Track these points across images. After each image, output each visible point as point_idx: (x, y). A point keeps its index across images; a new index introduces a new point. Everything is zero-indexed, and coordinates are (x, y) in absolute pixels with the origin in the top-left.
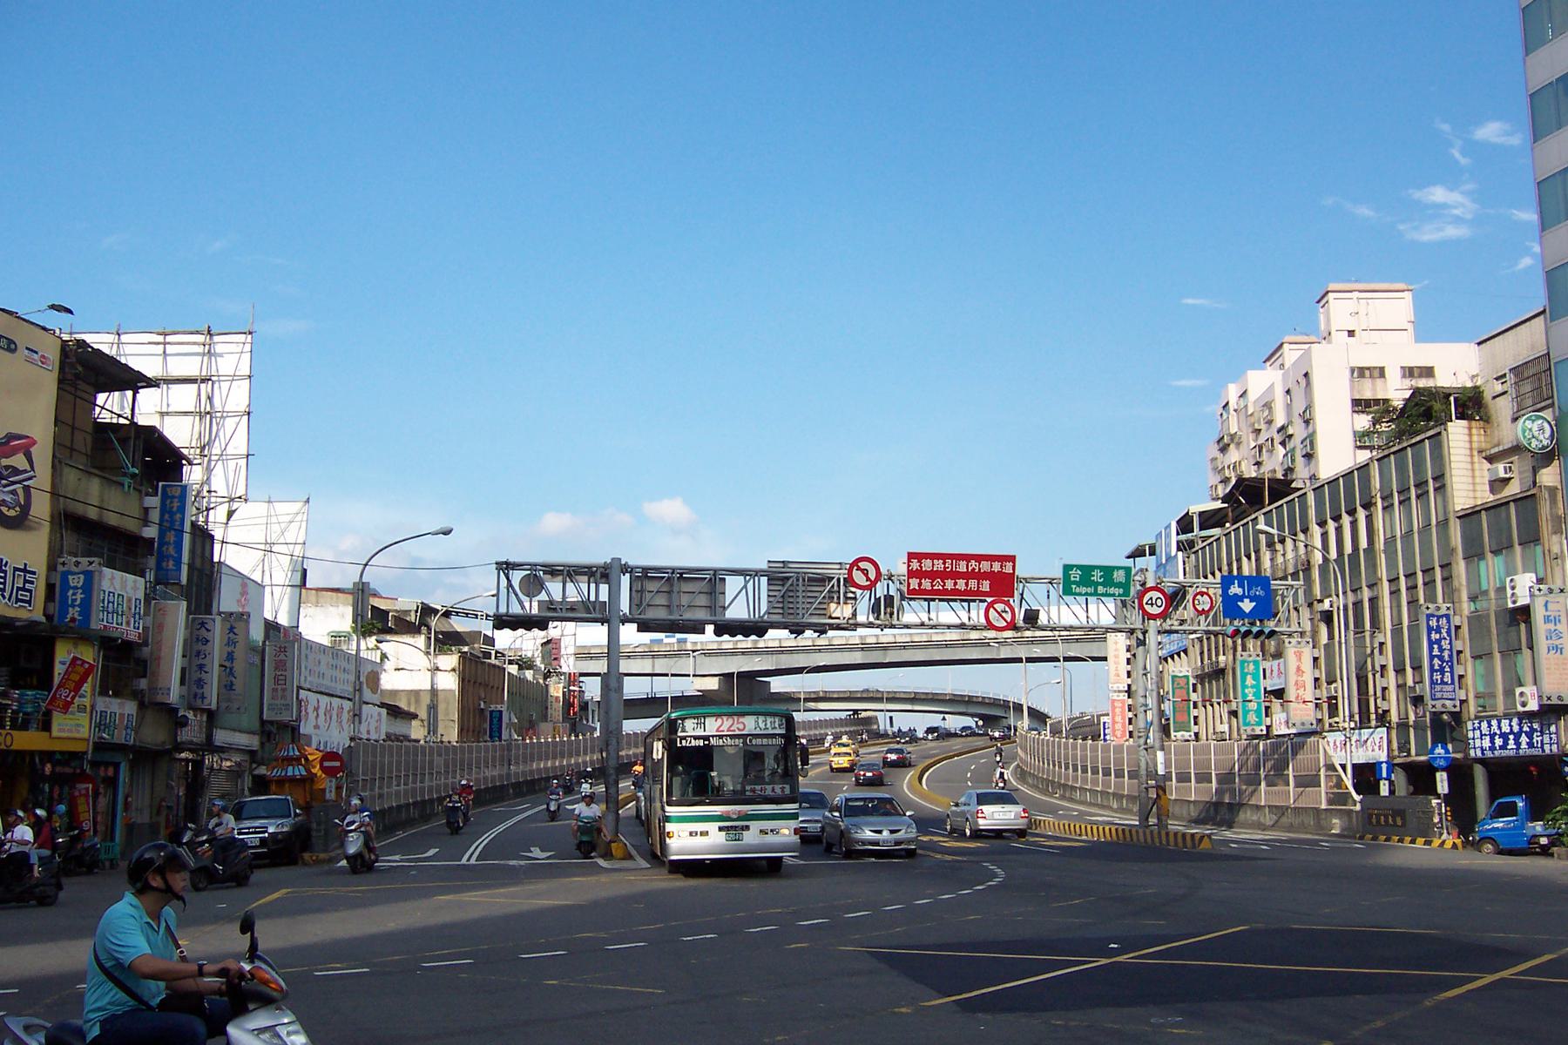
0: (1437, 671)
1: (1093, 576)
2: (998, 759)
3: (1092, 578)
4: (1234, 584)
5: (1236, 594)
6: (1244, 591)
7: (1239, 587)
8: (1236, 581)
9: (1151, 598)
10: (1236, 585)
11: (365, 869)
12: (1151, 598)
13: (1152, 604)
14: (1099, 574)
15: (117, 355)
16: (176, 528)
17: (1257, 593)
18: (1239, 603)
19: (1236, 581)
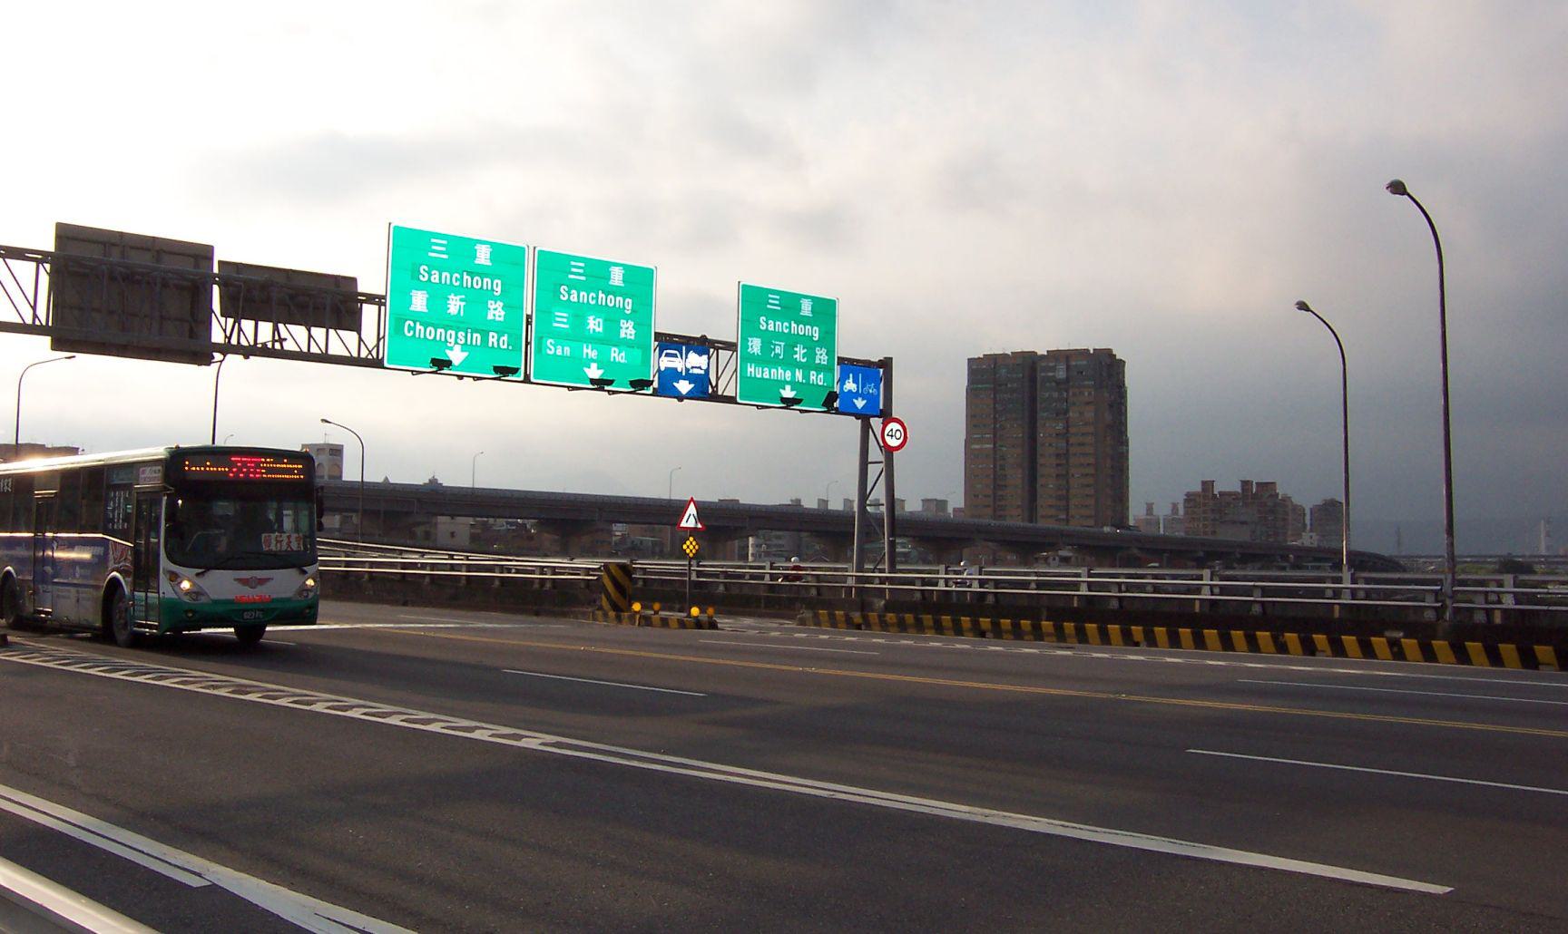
0: (277, 341)
1: (796, 354)
2: (97, 867)
3: (795, 357)
4: (849, 378)
5: (850, 391)
6: (858, 387)
7: (854, 382)
8: (851, 375)
9: (892, 430)
10: (851, 380)
11: (137, 277)
12: (892, 430)
13: (892, 436)
14: (802, 352)
15: (274, 341)
16: (998, 396)
17: (871, 391)
18: (675, 384)
19: (851, 375)
